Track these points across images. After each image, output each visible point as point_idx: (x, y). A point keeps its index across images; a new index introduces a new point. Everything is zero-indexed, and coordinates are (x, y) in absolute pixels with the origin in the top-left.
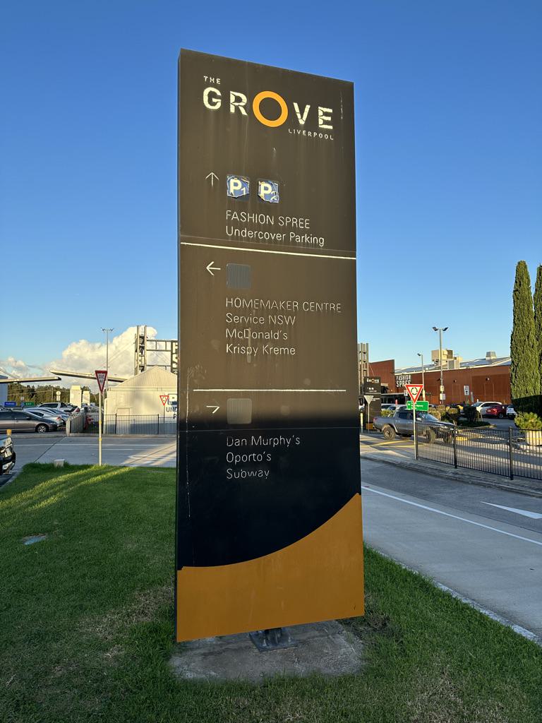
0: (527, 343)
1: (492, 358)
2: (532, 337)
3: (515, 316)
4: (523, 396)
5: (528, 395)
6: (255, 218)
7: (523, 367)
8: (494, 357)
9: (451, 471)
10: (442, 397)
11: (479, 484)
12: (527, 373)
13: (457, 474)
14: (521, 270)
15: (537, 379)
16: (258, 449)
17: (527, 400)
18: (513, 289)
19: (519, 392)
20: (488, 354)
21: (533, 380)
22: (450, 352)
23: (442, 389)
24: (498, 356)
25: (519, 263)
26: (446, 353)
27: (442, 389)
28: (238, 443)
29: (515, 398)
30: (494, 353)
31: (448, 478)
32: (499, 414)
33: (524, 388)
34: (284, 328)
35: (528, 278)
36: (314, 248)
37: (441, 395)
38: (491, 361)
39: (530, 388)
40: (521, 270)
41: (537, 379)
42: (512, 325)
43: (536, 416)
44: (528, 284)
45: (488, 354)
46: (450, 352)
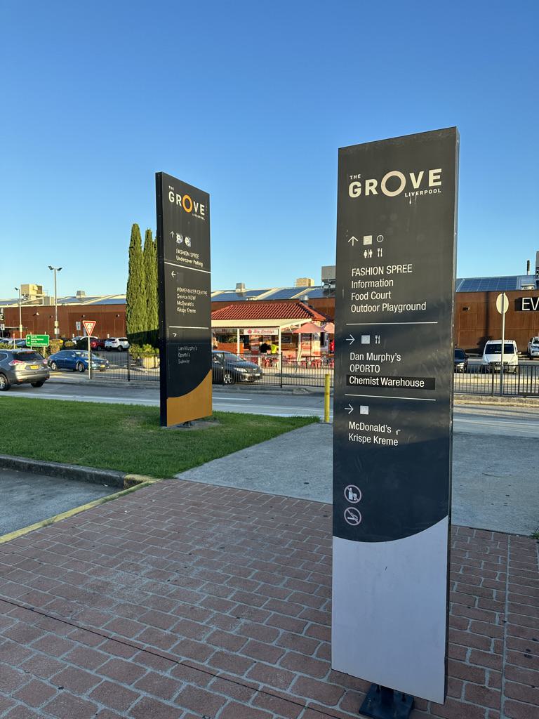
0: (139, 290)
1: (82, 296)
2: (143, 286)
3: (130, 268)
4: (136, 332)
5: (139, 331)
6: (184, 253)
7: (136, 309)
8: (84, 296)
9: (127, 383)
10: (56, 331)
11: (153, 389)
12: (139, 314)
13: (132, 384)
14: (135, 229)
15: (145, 319)
16: (186, 352)
17: (138, 335)
18: (129, 246)
19: (133, 328)
20: (79, 293)
21: (143, 319)
22: (40, 288)
23: (56, 324)
24: (88, 295)
25: (134, 225)
26: (36, 288)
27: (56, 324)
28: (181, 349)
29: (129, 333)
30: (84, 292)
31: (127, 388)
32: (97, 346)
33: (136, 326)
34: (192, 301)
35: (140, 238)
36: (199, 267)
37: (56, 329)
38: (80, 300)
39: (141, 326)
40: (135, 229)
41: (145, 319)
42: (128, 275)
43: (150, 346)
44: (140, 244)
45: (79, 293)
46: (40, 288)
